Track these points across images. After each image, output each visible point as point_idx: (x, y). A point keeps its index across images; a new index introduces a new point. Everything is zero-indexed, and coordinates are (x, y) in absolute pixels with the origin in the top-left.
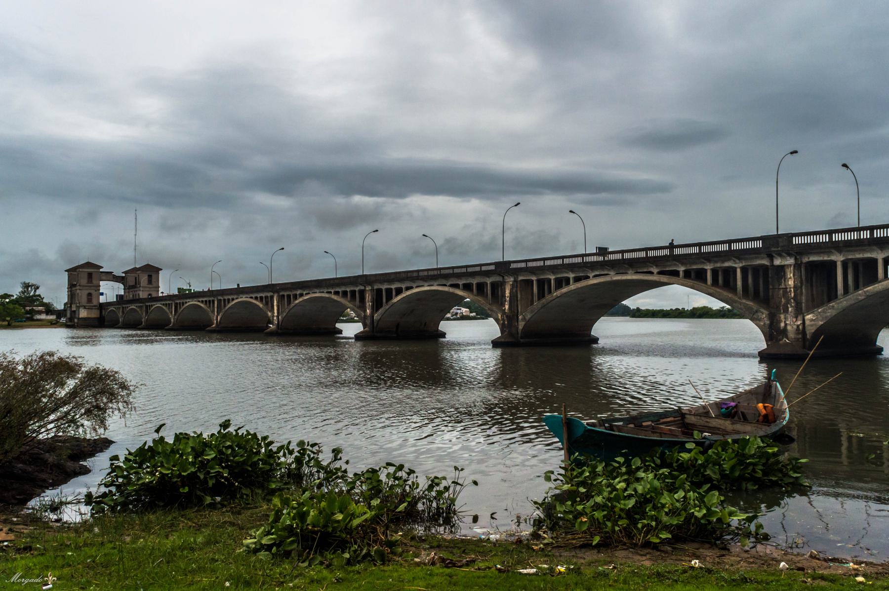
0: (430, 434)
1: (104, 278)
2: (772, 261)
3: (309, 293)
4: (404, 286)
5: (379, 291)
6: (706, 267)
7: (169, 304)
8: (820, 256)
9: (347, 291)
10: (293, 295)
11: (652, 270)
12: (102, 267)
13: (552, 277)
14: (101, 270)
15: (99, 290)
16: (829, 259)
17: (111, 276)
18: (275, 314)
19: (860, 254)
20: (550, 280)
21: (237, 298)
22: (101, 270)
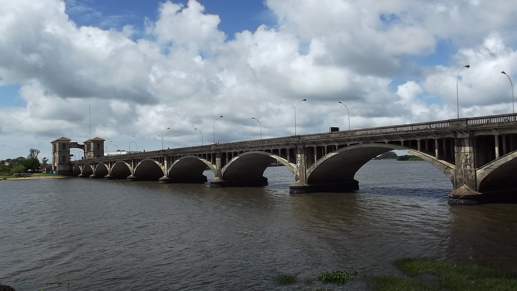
0: (184, 258)
1: (73, 146)
2: (456, 136)
3: (184, 156)
4: (143, 158)
5: (111, 161)
6: (417, 139)
7: (107, 162)
8: (485, 132)
9: (206, 154)
10: (175, 156)
11: (384, 141)
12: (71, 140)
13: (325, 146)
14: (70, 142)
15: (70, 154)
16: (490, 134)
17: (76, 145)
18: (165, 168)
19: (508, 131)
20: (325, 147)
21: (144, 159)
22: (70, 142)
